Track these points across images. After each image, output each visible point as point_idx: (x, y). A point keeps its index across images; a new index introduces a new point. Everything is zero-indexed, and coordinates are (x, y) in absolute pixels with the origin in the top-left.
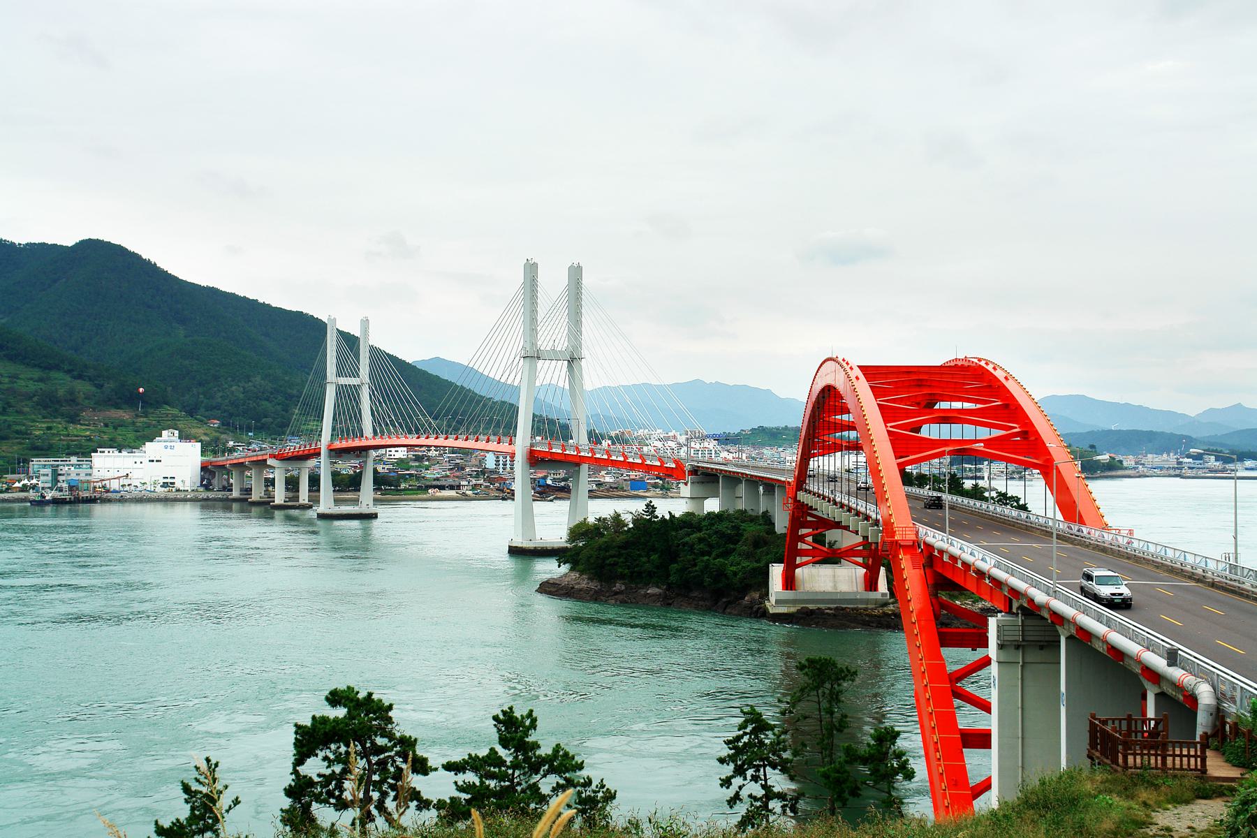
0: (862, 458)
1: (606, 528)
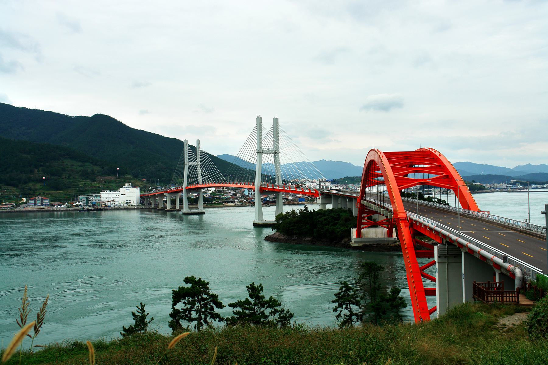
0: (385, 188)
1: (290, 216)
